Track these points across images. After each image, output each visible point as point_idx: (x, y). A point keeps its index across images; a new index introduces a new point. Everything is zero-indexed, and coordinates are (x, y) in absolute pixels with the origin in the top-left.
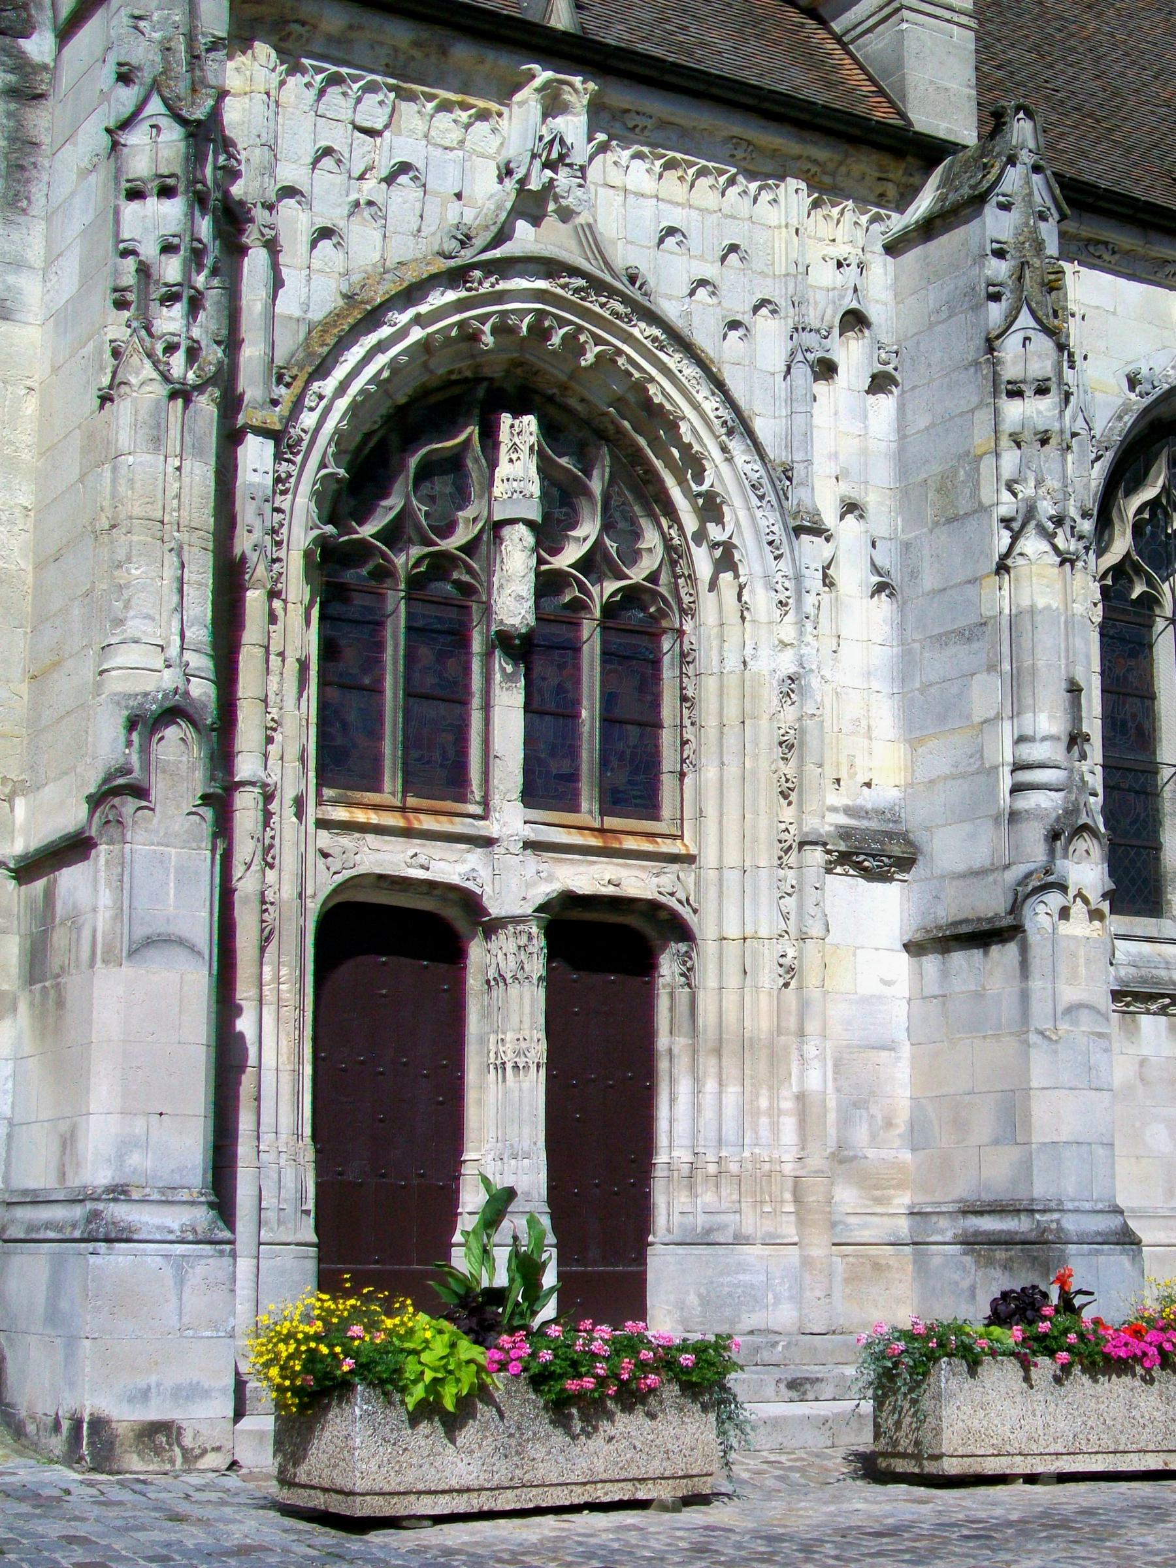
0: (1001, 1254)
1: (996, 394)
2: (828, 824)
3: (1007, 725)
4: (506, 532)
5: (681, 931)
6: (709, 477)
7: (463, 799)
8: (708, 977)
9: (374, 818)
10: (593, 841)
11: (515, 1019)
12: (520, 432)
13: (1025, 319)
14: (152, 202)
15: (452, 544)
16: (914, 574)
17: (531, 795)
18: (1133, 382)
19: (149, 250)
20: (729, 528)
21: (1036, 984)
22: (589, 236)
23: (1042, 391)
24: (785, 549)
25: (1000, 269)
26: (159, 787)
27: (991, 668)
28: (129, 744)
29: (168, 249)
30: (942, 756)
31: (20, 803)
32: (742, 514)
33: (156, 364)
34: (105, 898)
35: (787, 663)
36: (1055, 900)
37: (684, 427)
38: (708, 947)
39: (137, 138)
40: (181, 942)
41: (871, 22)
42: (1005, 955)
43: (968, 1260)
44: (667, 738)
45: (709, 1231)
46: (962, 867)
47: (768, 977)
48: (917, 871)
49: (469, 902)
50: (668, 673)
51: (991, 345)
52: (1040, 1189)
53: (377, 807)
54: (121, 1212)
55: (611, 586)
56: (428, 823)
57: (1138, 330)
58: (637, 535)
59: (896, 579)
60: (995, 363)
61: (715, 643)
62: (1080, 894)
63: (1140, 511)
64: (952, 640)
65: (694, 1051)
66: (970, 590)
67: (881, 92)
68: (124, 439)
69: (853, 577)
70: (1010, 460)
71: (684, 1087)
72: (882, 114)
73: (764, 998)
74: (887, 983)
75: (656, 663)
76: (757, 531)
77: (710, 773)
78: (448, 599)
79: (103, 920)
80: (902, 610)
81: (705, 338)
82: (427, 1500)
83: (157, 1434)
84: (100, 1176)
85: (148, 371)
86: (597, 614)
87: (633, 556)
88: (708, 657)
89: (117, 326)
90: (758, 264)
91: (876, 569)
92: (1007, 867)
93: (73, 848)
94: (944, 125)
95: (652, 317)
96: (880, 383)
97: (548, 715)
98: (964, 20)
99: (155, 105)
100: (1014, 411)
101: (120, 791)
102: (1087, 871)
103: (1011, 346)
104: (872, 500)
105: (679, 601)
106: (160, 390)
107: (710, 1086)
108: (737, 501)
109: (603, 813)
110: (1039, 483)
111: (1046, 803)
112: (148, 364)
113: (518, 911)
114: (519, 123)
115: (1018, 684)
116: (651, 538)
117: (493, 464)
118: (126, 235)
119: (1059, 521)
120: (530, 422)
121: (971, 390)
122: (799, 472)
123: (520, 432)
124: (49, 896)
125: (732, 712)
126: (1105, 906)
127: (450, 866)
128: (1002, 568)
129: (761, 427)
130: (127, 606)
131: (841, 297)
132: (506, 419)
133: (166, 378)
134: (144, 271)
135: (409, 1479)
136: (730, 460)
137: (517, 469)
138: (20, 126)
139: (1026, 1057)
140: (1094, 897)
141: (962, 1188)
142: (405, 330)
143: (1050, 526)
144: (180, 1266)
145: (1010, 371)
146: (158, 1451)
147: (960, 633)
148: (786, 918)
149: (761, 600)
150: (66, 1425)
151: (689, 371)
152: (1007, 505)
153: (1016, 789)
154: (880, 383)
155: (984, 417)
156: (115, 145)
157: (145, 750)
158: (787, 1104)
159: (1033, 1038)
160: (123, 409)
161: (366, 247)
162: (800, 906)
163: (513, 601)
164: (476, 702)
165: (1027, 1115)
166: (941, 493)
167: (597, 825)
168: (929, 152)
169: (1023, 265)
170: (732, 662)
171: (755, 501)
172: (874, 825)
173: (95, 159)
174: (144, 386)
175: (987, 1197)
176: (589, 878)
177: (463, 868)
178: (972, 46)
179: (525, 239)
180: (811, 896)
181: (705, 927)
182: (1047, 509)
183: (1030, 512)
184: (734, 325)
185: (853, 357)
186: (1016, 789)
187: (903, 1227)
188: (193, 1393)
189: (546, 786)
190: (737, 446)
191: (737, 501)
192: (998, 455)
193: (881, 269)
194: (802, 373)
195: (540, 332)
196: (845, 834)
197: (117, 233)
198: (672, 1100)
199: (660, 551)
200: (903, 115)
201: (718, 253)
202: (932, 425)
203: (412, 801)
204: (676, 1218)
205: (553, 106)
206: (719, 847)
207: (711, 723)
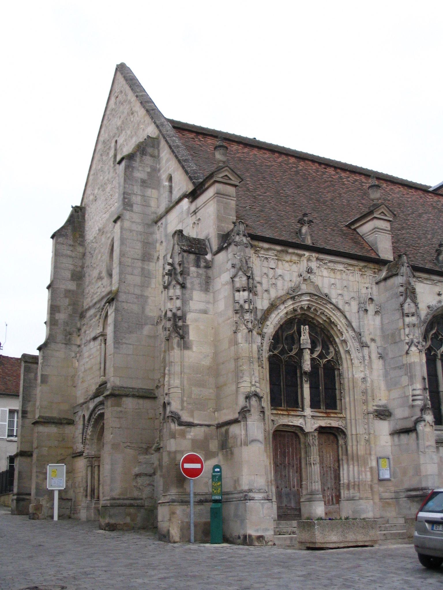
0: (416, 499)
1: (403, 316)
2: (371, 409)
3: (410, 387)
4: (304, 351)
5: (344, 433)
6: (344, 336)
7: (297, 407)
8: (350, 443)
9: (282, 413)
10: (325, 415)
11: (312, 453)
12: (305, 330)
13: (409, 300)
14: (241, 293)
15: (293, 353)
16: (387, 354)
17: (312, 406)
18: (429, 307)
19: (242, 302)
20: (349, 347)
21: (420, 441)
22: (317, 287)
23: (413, 315)
24: (360, 351)
25: (402, 289)
26: (252, 410)
27: (406, 375)
28: (246, 402)
29: (245, 302)
30: (396, 394)
31: (216, 413)
32: (351, 344)
33: (245, 325)
34: (243, 432)
35: (362, 375)
36: (423, 423)
37: (338, 326)
38: (349, 436)
39: (237, 279)
40: (258, 441)
41: (369, 233)
42: (413, 435)
43: (409, 501)
44: (337, 392)
45: (353, 497)
46: (401, 417)
47: (363, 443)
48: (392, 418)
49: (301, 429)
50: (337, 378)
51: (402, 305)
52: (424, 485)
53: (282, 410)
54: (251, 495)
55: (325, 360)
56: (292, 413)
57: (429, 295)
58: (329, 349)
59: (383, 355)
60: (402, 310)
61: (346, 371)
62: (428, 422)
63: (432, 335)
64: (396, 368)
65: (348, 460)
66: (400, 358)
67: (372, 249)
68: (240, 341)
69: (374, 356)
70: (407, 330)
71: (345, 467)
72: (373, 256)
73: (362, 447)
74: (387, 443)
75: (334, 377)
76: (354, 347)
77: (347, 399)
78: (295, 365)
79: (243, 437)
80: (384, 362)
81: (340, 307)
82: (331, 544)
83: (260, 538)
84: (245, 487)
85: (244, 327)
86: (322, 366)
87: (328, 353)
88: (345, 375)
89: (236, 318)
90: (351, 289)
91: (379, 354)
92: (412, 417)
93: (236, 421)
94: (386, 256)
95: (331, 303)
96: (377, 312)
97: (314, 388)
98: (388, 232)
99: (240, 273)
100: (407, 320)
101: (244, 412)
102: (429, 417)
103: (406, 306)
104: (378, 339)
105: (338, 362)
106: (246, 331)
107: (351, 466)
108: (350, 341)
109: (326, 409)
110: (413, 335)
111: (419, 403)
112: (244, 325)
113: (311, 431)
114: (303, 265)
115: (411, 378)
116: (332, 349)
117: (300, 336)
118: (236, 299)
119: (418, 343)
120: (307, 327)
121: (398, 315)
122: (362, 333)
123: (305, 330)
124: (227, 432)
125: (351, 388)
126: (433, 424)
127: (298, 422)
128: (407, 353)
129: (354, 324)
130: (243, 374)
131: (368, 295)
132: (302, 326)
133: (248, 328)
134: (241, 306)
135: (325, 540)
136: (348, 332)
137: (305, 337)
138: (207, 274)
139: (419, 457)
140: (431, 422)
141: (406, 486)
143: (417, 344)
144: (262, 504)
145: (406, 311)
146: (261, 541)
147: (398, 367)
148: (365, 429)
149: (356, 362)
150: (242, 537)
151: (339, 314)
152: (407, 340)
153: (413, 400)
154: (377, 312)
155: (401, 320)
156: (233, 281)
157: (250, 403)
158: (368, 469)
159: (420, 453)
160: (239, 335)
161: (273, 294)
162: (368, 427)
163: (307, 366)
164: (299, 387)
165: (420, 469)
166: (391, 337)
167: (325, 411)
168: (382, 263)
169: (407, 288)
170: (350, 376)
171: (354, 341)
172: (382, 408)
173: (181, 255)
174: (243, 330)
175: (412, 487)
176: (323, 423)
177: (299, 422)
178: (391, 238)
179: (304, 288)
180: (371, 425)
181: (349, 433)
182: (415, 341)
183: (412, 342)
184: (347, 303)
185: (371, 308)
186: (413, 400)
187: (393, 495)
188: (266, 530)
189: (314, 405)
190: (350, 330)
191: (350, 341)
192: (404, 329)
193: (375, 287)
194: (362, 313)
195: (309, 308)
196: (376, 411)
197: (234, 299)
198: (343, 469)
199: (334, 352)
200: (378, 255)
201: (341, 285)
202: (389, 322)
203: (288, 408)
204: (346, 495)
205: (309, 260)
206: (352, 415)
207: (346, 388)
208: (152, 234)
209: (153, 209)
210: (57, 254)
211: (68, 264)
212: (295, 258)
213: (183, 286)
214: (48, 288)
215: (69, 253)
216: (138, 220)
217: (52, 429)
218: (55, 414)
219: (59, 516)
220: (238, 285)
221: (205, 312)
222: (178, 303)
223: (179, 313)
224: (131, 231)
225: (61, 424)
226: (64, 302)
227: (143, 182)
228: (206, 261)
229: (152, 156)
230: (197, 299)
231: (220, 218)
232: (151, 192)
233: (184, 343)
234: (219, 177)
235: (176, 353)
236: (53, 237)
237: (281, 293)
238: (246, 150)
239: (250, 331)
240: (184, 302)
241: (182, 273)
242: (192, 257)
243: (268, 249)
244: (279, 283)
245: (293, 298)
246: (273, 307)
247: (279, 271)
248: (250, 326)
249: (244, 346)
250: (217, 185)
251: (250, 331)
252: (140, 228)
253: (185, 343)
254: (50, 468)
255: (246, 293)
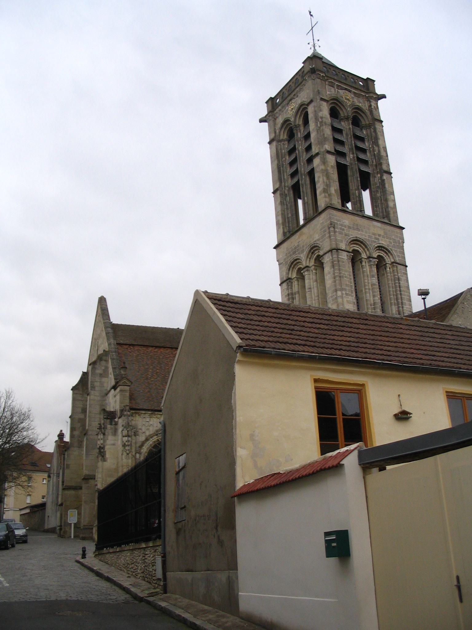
128: (311, 15)
142: (151, 442)
161: (148, 433)
174: (125, 454)
208: (105, 400)
209: (105, 388)
210: (74, 400)
211: (80, 404)
212: (159, 416)
213: (104, 434)
214: (70, 417)
215: (80, 398)
216: (98, 394)
217: (72, 492)
218: (73, 484)
219: (74, 537)
220: (124, 434)
221: (114, 445)
222: (102, 442)
223: (102, 446)
224: (94, 400)
225: (77, 489)
226: (78, 425)
227: (101, 375)
228: (115, 422)
229: (106, 361)
230: (110, 439)
231: (121, 402)
232: (104, 380)
233: (104, 459)
234: (121, 383)
235: (100, 463)
236: (72, 390)
237: (151, 433)
238: (156, 350)
239: (128, 454)
240: (105, 441)
241: (104, 428)
242: (108, 420)
243: (145, 414)
244: (151, 428)
245: (157, 435)
246: (147, 440)
247: (151, 423)
248: (128, 452)
249: (125, 460)
250: (121, 387)
251: (128, 454)
252: (99, 398)
253: (104, 459)
254: (69, 512)
255: (127, 438)
